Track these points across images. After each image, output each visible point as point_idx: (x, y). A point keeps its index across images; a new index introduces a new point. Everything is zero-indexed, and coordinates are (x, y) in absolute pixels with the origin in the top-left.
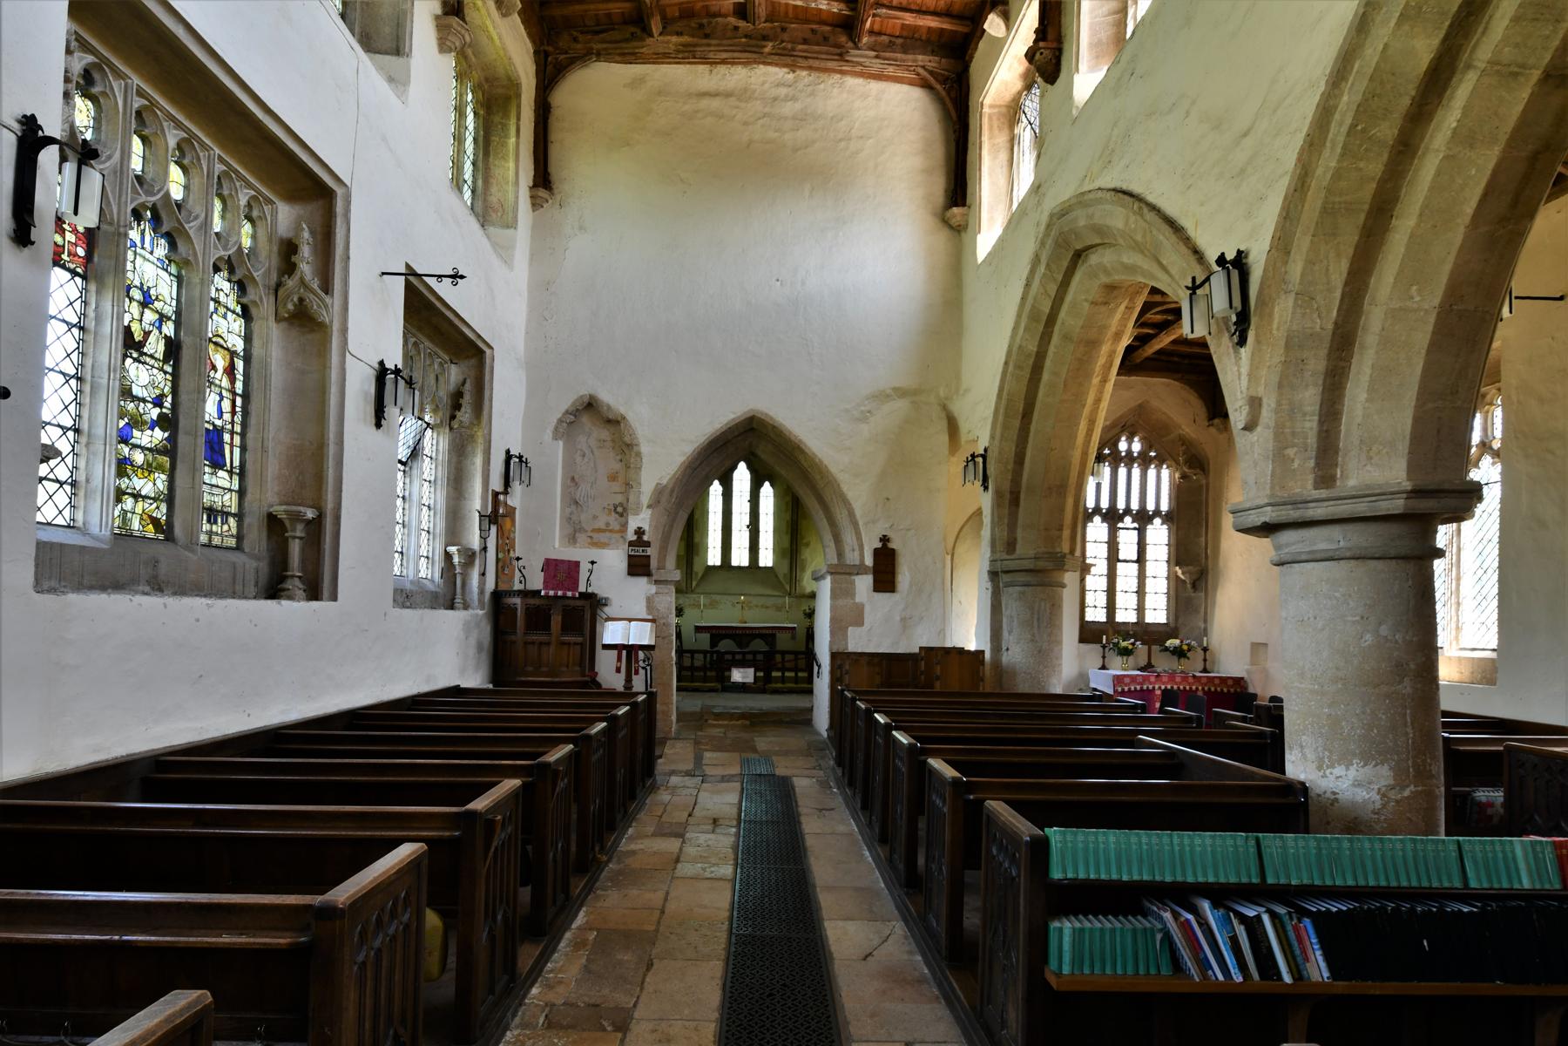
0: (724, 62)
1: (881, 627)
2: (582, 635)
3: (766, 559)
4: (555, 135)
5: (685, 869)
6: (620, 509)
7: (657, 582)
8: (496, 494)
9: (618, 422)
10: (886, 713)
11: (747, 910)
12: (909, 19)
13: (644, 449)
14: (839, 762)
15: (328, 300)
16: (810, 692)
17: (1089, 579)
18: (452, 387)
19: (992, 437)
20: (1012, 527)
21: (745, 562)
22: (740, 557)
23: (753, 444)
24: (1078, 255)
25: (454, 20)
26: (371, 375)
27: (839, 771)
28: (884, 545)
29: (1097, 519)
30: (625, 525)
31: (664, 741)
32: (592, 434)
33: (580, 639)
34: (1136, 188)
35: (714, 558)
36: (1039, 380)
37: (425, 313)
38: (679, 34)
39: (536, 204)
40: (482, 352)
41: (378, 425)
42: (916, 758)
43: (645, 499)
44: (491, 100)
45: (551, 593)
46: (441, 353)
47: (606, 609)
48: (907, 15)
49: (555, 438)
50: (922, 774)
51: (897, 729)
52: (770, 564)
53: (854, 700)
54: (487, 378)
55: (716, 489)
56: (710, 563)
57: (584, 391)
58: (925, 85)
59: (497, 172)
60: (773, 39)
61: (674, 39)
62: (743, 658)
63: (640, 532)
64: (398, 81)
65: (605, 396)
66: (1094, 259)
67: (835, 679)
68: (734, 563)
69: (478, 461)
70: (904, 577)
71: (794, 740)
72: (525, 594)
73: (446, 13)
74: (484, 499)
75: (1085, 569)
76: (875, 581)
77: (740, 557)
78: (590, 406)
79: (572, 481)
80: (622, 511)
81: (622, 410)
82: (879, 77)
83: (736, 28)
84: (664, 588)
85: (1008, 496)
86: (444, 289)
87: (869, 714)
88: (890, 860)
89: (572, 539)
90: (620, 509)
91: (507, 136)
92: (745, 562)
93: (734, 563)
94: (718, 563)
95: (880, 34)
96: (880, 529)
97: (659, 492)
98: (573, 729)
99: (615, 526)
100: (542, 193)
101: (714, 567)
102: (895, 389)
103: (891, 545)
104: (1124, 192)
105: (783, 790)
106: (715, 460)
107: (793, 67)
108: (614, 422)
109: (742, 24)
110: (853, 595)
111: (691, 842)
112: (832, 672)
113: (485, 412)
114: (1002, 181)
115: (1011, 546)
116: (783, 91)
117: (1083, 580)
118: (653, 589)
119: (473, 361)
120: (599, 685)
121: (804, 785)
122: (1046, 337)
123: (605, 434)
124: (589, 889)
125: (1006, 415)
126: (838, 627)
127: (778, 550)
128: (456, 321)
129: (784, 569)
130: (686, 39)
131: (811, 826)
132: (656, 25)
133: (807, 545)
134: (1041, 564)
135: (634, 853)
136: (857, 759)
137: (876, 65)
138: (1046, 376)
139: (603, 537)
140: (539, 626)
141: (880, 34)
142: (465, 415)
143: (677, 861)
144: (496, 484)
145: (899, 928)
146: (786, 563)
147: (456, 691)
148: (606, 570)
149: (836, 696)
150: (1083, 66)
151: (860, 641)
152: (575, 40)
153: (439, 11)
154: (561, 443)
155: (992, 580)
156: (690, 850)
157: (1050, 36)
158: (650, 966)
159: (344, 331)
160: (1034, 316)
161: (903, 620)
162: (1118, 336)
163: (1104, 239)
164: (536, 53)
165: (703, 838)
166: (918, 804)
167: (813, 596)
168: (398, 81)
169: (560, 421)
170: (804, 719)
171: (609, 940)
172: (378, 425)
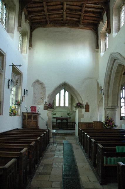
0: (59, 27)
1: (87, 118)
2: (36, 120)
3: (67, 105)
4: (32, 37)
5: (55, 156)
6: (42, 98)
7: (49, 111)
8: (23, 97)
9: (42, 84)
10: (87, 133)
11: (66, 174)
12: (88, 21)
13: (47, 88)
14: (80, 141)
15: (3, 70)
16: (75, 129)
17: (122, 109)
18: (16, 80)
19: (104, 87)
20: (108, 101)
21: (63, 106)
22: (62, 105)
23: (65, 86)
24: (115, 60)
25: (20, 27)
26: (8, 80)
27: (79, 142)
28: (87, 104)
29: (123, 99)
30: (43, 101)
31: (51, 137)
32: (38, 86)
33: (36, 121)
34: (120, 53)
35: (57, 105)
36: (111, 78)
37: (16, 71)
38: (52, 23)
39: (29, 49)
40: (21, 74)
41: (8, 88)
42: (90, 138)
43: (47, 97)
44: (23, 34)
45: (32, 112)
46: (15, 74)
47: (40, 115)
48: (88, 20)
49: (32, 87)
50: (97, 146)
51: (98, 143)
52: (67, 106)
53: (82, 131)
54: (22, 78)
55: (58, 95)
56: (57, 106)
57: (37, 79)
58: (91, 30)
59: (24, 45)
60: (67, 24)
61: (51, 24)
62: (64, 124)
63: (46, 102)
64: (12, 37)
65: (40, 80)
66: (117, 61)
67: (79, 127)
68: (61, 106)
69: (20, 91)
70: (90, 110)
71: (72, 138)
72: (27, 113)
73: (19, 26)
74: (21, 97)
75: (121, 107)
76: (86, 110)
77: (62, 105)
78: (38, 81)
79: (35, 94)
80: (42, 99)
81: (43, 82)
82: (84, 29)
83: (61, 22)
84: (50, 112)
85: (107, 96)
86: (18, 67)
87: (84, 133)
88: (91, 162)
89: (34, 104)
90: (42, 98)
91: (25, 40)
92: (63, 106)
93: (61, 106)
94: (58, 106)
95: (84, 23)
96: (86, 101)
97: (49, 95)
98: (39, 135)
99: (42, 101)
100: (30, 48)
101: (57, 107)
102: (88, 78)
103: (88, 104)
104: (120, 54)
105: (70, 145)
106: (57, 90)
107: (70, 27)
108: (41, 84)
109: (62, 22)
110: (82, 113)
111: (57, 154)
112: (79, 126)
113: (21, 83)
114: (117, 22)
115: (107, 104)
116: (69, 31)
117: (120, 109)
118: (48, 112)
119: (20, 75)
120: (39, 128)
121: (74, 146)
122: (111, 72)
123: (40, 86)
124: (38, 167)
125: (106, 83)
126: (79, 118)
127: (69, 104)
128: (18, 70)
129: (70, 107)
130: (53, 24)
131: (75, 151)
132: (49, 22)
133: (74, 102)
134: (113, 107)
135: (47, 154)
136: (82, 140)
137: (83, 27)
138: (112, 77)
139: (40, 103)
140: (30, 117)
141: (84, 23)
142: (18, 84)
143: (54, 156)
144: (23, 95)
145: (88, 164)
146: (70, 105)
147: (17, 129)
148: (40, 108)
149: (79, 130)
150: (114, 32)
151: (83, 120)
152: (36, 25)
153: (18, 26)
154: (33, 88)
155: (105, 110)
156: (56, 154)
157: (109, 28)
158: (52, 168)
159: (5, 75)
160: (109, 68)
161: (90, 117)
162: (122, 71)
163: (118, 59)
164: (30, 27)
165: (58, 152)
166: (96, 152)
167: (75, 112)
168: (12, 37)
169: (33, 84)
170: (73, 134)
171: (47, 165)
172: (8, 88)
